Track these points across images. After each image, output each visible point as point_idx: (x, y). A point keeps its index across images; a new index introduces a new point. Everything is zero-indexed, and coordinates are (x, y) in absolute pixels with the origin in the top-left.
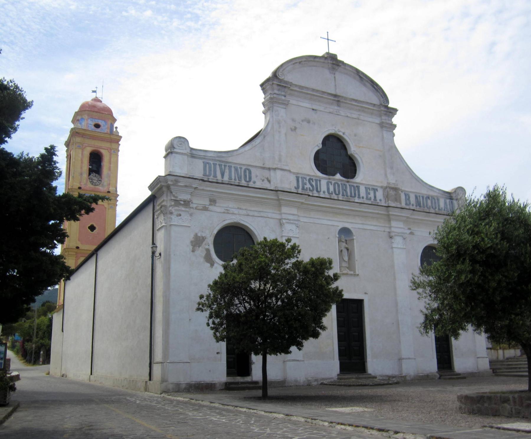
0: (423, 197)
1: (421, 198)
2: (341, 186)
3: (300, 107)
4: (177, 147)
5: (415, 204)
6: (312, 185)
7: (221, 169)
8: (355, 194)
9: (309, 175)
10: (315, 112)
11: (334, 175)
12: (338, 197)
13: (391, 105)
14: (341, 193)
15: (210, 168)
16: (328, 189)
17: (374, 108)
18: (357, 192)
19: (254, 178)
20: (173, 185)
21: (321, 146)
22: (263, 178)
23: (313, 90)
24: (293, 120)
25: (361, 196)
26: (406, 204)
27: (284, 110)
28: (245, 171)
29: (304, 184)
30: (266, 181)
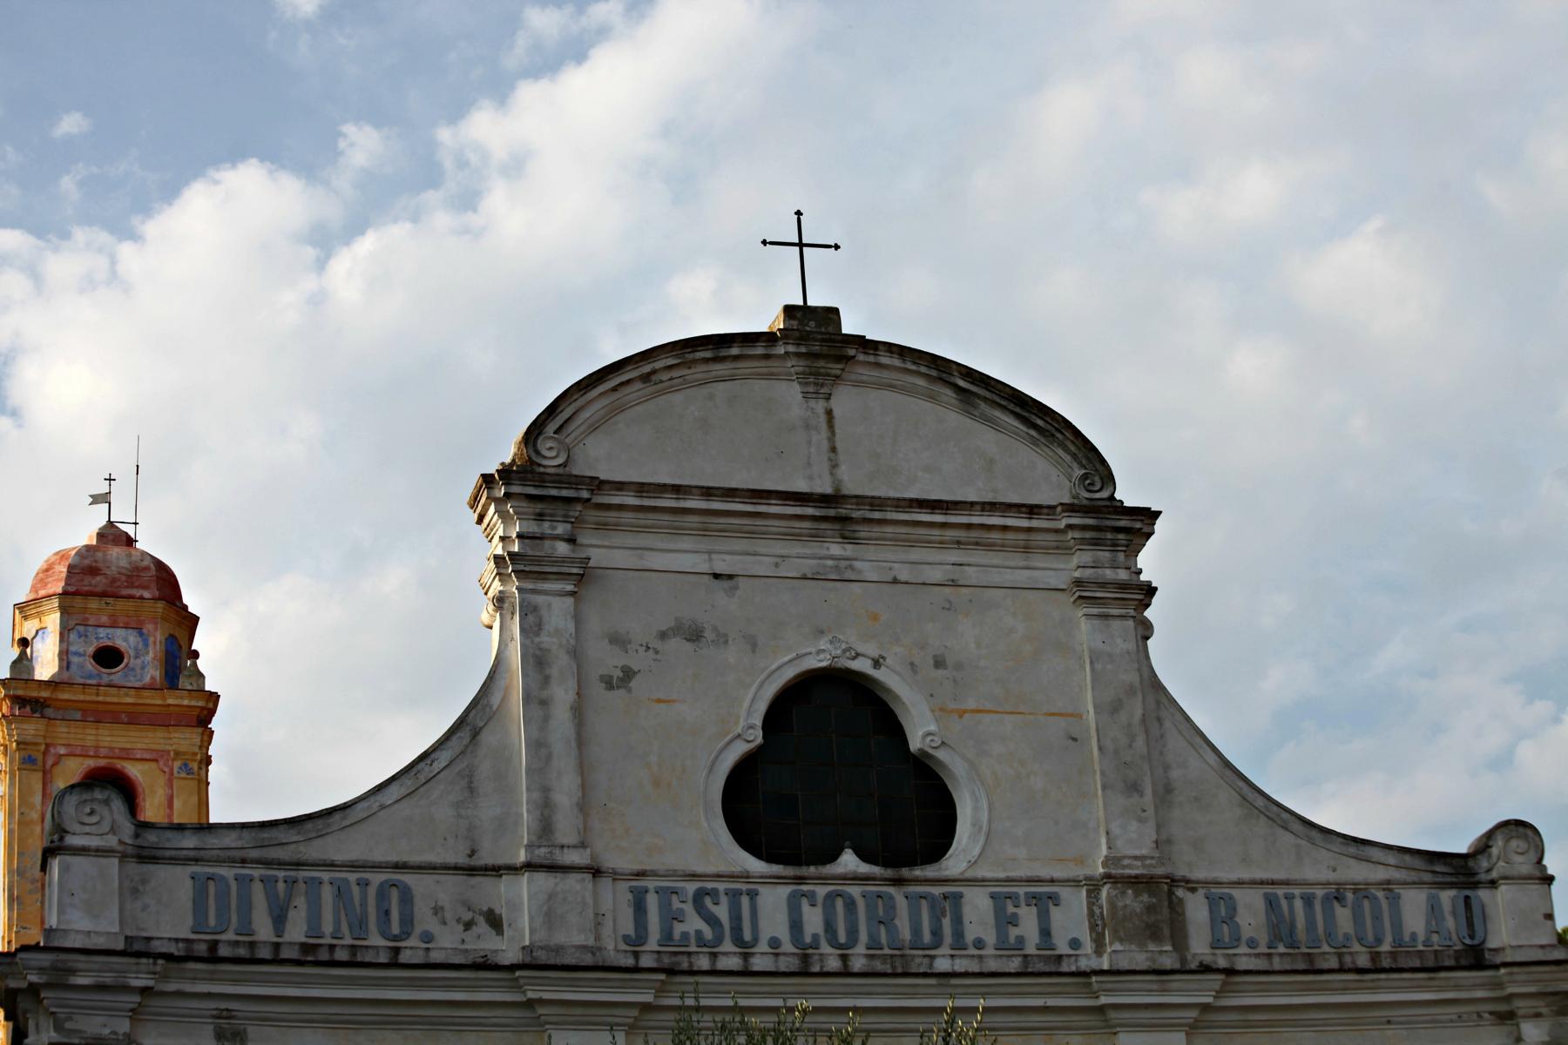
0: (1308, 901)
1: (1298, 904)
2: (861, 905)
3: (654, 569)
4: (77, 828)
5: (1263, 939)
6: (713, 921)
7: (271, 896)
8: (937, 933)
9: (693, 876)
10: (726, 584)
11: (833, 857)
12: (844, 958)
13: (1128, 495)
14: (863, 937)
15: (223, 897)
16: (796, 926)
17: (1035, 523)
18: (946, 922)
19: (425, 920)
20: (49, 986)
21: (757, 737)
22: (467, 916)
23: (708, 492)
24: (619, 641)
25: (970, 937)
26: (1216, 944)
27: (570, 600)
28: (382, 894)
29: (671, 918)
30: (482, 927)
